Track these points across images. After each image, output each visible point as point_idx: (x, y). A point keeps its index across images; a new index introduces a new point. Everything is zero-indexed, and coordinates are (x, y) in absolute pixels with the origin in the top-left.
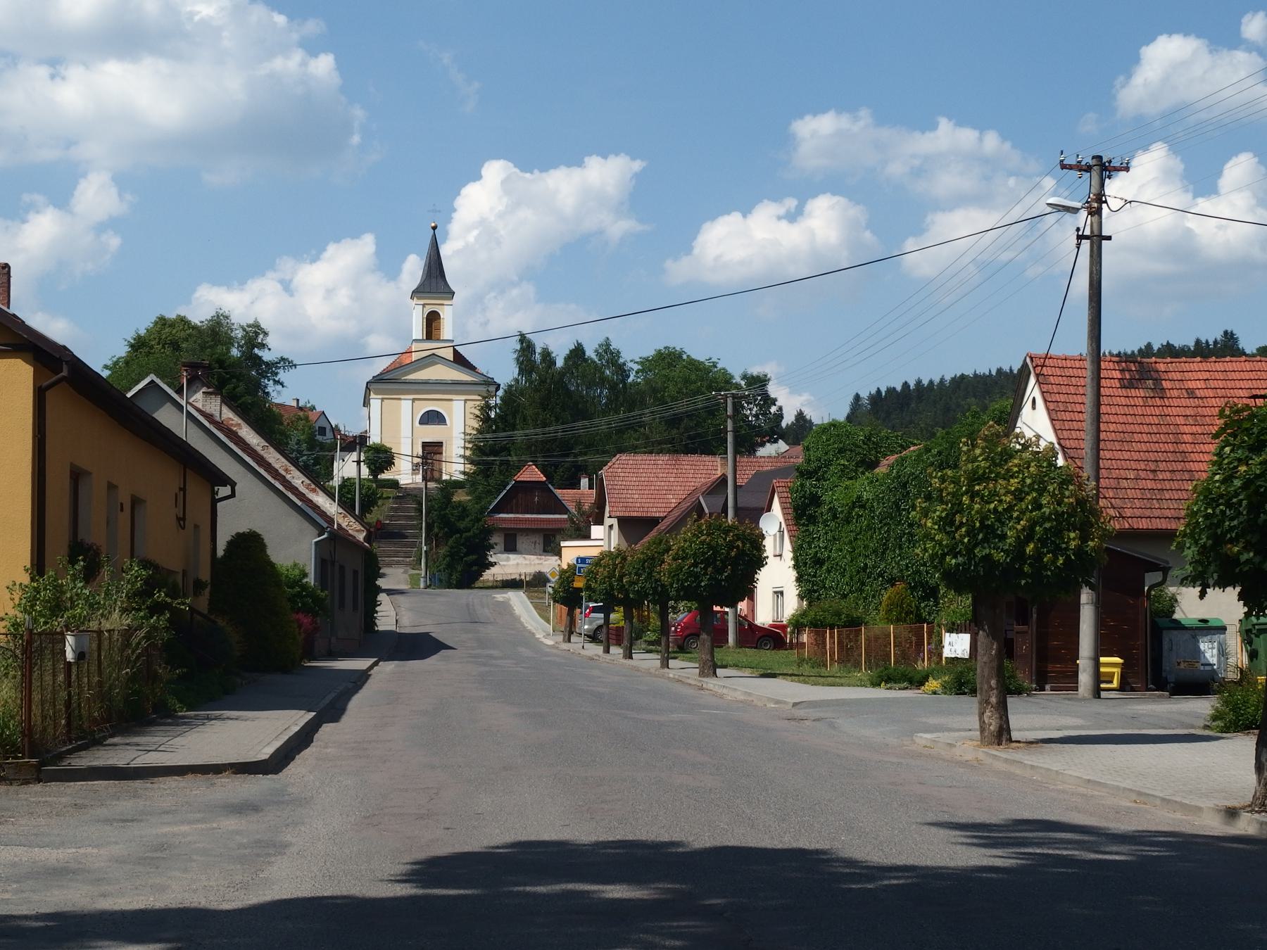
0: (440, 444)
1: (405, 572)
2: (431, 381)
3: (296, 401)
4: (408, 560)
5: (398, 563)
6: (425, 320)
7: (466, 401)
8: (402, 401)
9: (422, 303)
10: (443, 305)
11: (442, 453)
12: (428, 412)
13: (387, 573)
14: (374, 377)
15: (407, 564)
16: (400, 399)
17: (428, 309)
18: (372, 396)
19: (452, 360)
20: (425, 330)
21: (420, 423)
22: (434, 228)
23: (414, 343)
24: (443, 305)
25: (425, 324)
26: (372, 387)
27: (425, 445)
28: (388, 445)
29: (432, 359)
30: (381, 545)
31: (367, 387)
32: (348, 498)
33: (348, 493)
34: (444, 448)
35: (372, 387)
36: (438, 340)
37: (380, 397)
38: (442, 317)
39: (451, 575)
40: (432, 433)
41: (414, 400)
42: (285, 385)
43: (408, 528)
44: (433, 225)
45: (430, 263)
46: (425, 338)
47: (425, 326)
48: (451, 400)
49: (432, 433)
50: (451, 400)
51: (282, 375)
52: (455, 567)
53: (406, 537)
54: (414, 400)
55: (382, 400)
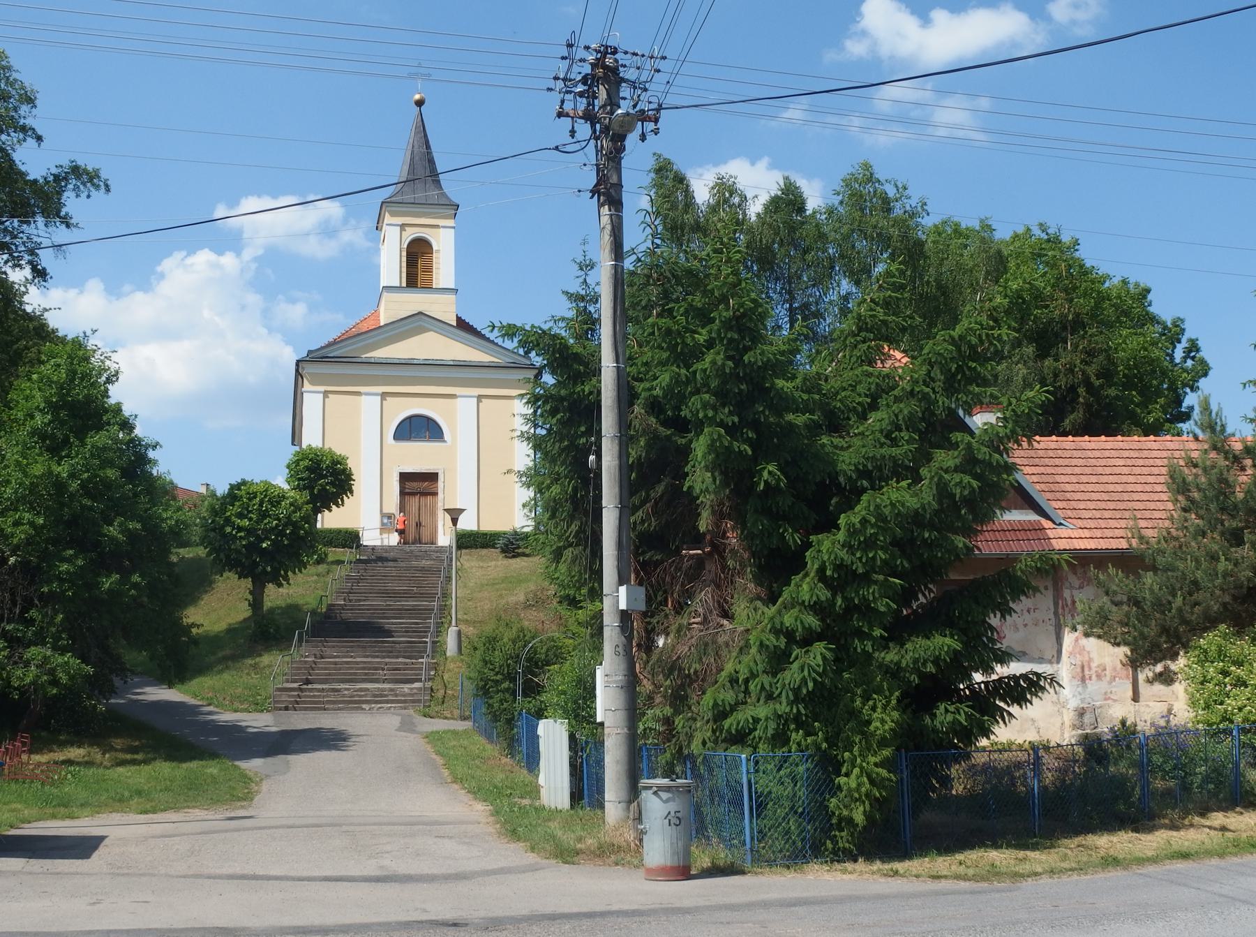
0: (432, 477)
1: (407, 726)
2: (415, 362)
3: (205, 487)
4: (406, 688)
5: (378, 698)
6: (404, 254)
7: (480, 398)
8: (363, 397)
9: (400, 223)
10: (437, 226)
11: (435, 494)
12: (410, 418)
13: (351, 730)
14: (310, 352)
15: (405, 702)
16: (358, 394)
17: (411, 234)
18: (307, 386)
19: (454, 324)
20: (404, 270)
21: (395, 438)
22: (420, 103)
23: (385, 294)
24: (437, 226)
25: (404, 259)
26: (308, 369)
27: (405, 478)
28: (339, 450)
29: (418, 322)
30: (328, 651)
31: (297, 371)
32: (240, 529)
33: (241, 516)
34: (440, 484)
35: (308, 369)
36: (428, 288)
37: (322, 388)
38: (435, 248)
39: (828, 766)
40: (418, 457)
41: (384, 396)
42: (73, 221)
43: (389, 613)
44: (417, 97)
45: (412, 159)
46: (404, 284)
47: (404, 264)
48: (453, 396)
49: (418, 457)
50: (453, 396)
51: (72, 203)
52: (853, 714)
53: (389, 633)
54: (384, 396)
55: (326, 394)
